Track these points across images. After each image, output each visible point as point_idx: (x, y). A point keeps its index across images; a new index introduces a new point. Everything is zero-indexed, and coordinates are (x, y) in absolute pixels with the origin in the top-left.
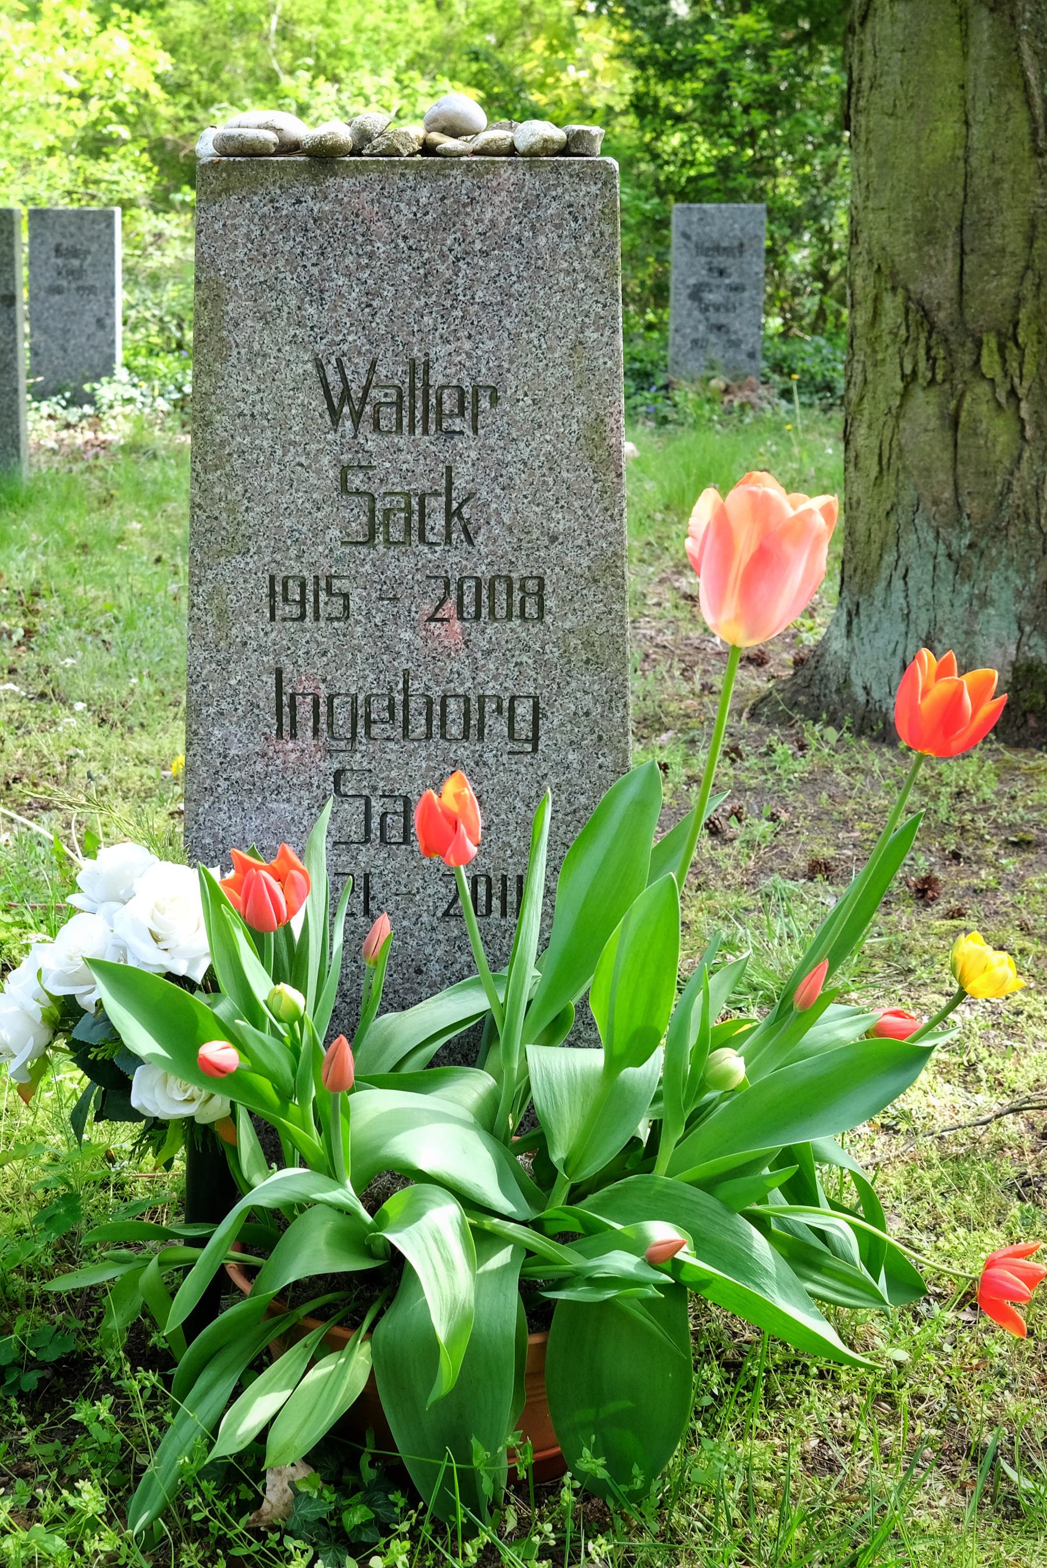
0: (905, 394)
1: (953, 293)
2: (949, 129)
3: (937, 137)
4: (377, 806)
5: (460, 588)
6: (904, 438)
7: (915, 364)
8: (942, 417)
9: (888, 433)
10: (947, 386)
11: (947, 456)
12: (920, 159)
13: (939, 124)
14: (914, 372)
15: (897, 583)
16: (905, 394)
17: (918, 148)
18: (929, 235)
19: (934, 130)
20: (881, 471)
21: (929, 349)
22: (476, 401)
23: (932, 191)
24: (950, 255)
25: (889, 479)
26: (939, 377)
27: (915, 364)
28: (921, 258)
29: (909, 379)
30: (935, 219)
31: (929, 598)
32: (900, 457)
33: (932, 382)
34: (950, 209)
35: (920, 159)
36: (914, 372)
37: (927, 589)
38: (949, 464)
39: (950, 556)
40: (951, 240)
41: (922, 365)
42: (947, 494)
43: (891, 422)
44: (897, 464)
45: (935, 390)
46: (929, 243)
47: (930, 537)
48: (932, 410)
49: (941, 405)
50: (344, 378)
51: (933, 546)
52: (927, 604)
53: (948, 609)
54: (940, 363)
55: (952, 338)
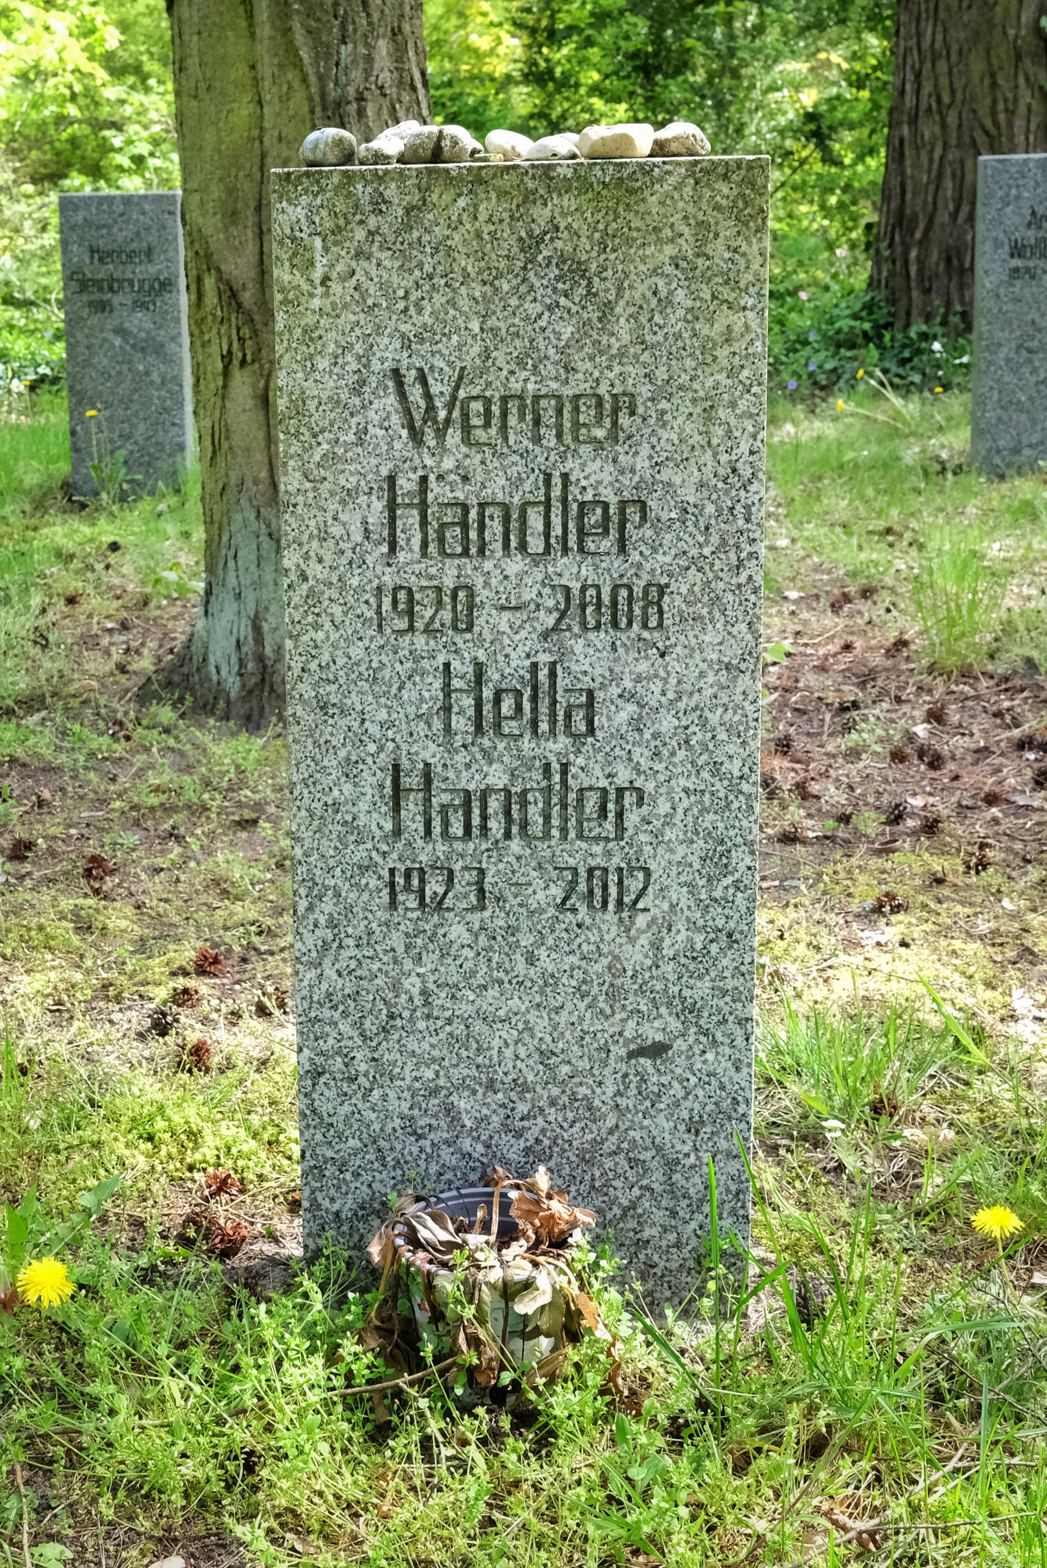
0: (226, 373)
1: (253, 273)
2: (243, 111)
3: (233, 118)
4: (609, 825)
5: (454, 597)
6: (230, 417)
7: (230, 345)
8: (254, 397)
9: (217, 413)
10: (257, 365)
11: (261, 435)
12: (220, 141)
13: (235, 105)
14: (230, 352)
15: (231, 563)
16: (226, 373)
17: (219, 130)
18: (233, 216)
19: (230, 111)
20: (214, 452)
21: (238, 330)
22: (504, 414)
23: (233, 173)
24: (250, 233)
25: (220, 459)
26: (249, 357)
27: (230, 345)
28: (227, 239)
29: (227, 358)
30: (236, 200)
31: (256, 578)
32: (227, 438)
33: (243, 363)
34: (247, 188)
35: (220, 141)
36: (230, 352)
37: (253, 568)
38: (263, 443)
39: (270, 535)
40: (251, 220)
41: (236, 345)
42: (264, 474)
43: (219, 403)
44: (225, 445)
45: (248, 369)
46: (234, 223)
47: (252, 516)
48: (247, 390)
49: (254, 385)
50: (428, 396)
51: (255, 526)
52: (253, 583)
53: (271, 588)
54: (248, 343)
55: (257, 317)
